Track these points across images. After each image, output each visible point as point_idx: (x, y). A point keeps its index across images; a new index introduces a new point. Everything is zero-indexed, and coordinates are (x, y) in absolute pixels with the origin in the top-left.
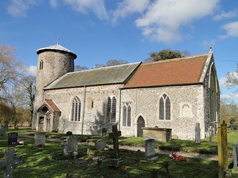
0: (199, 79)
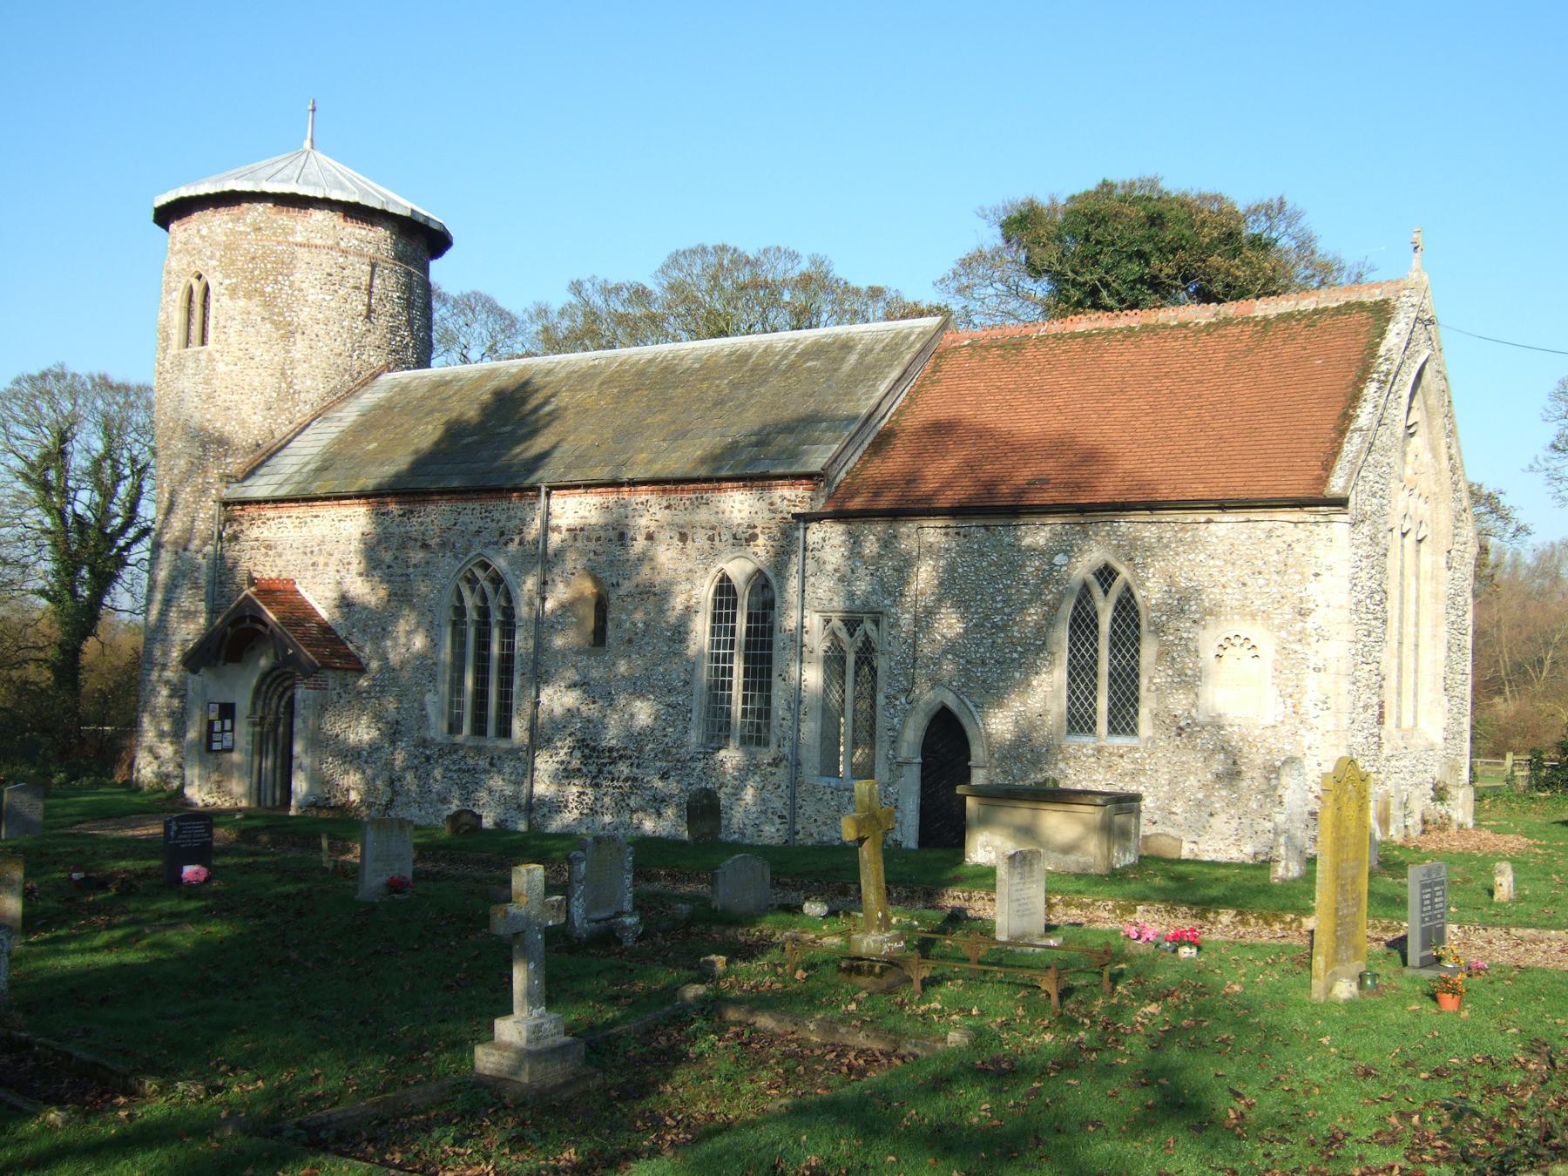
0: (1323, 481)
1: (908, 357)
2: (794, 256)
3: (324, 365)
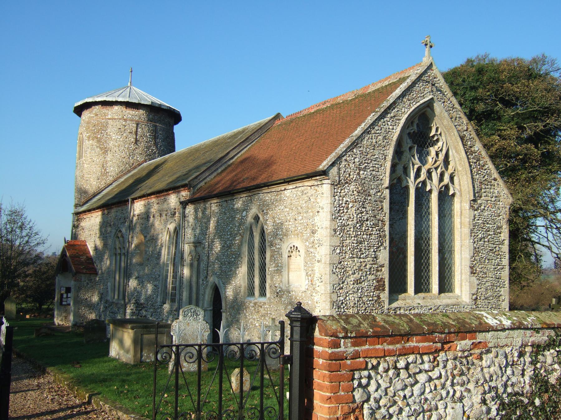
3: (118, 162)
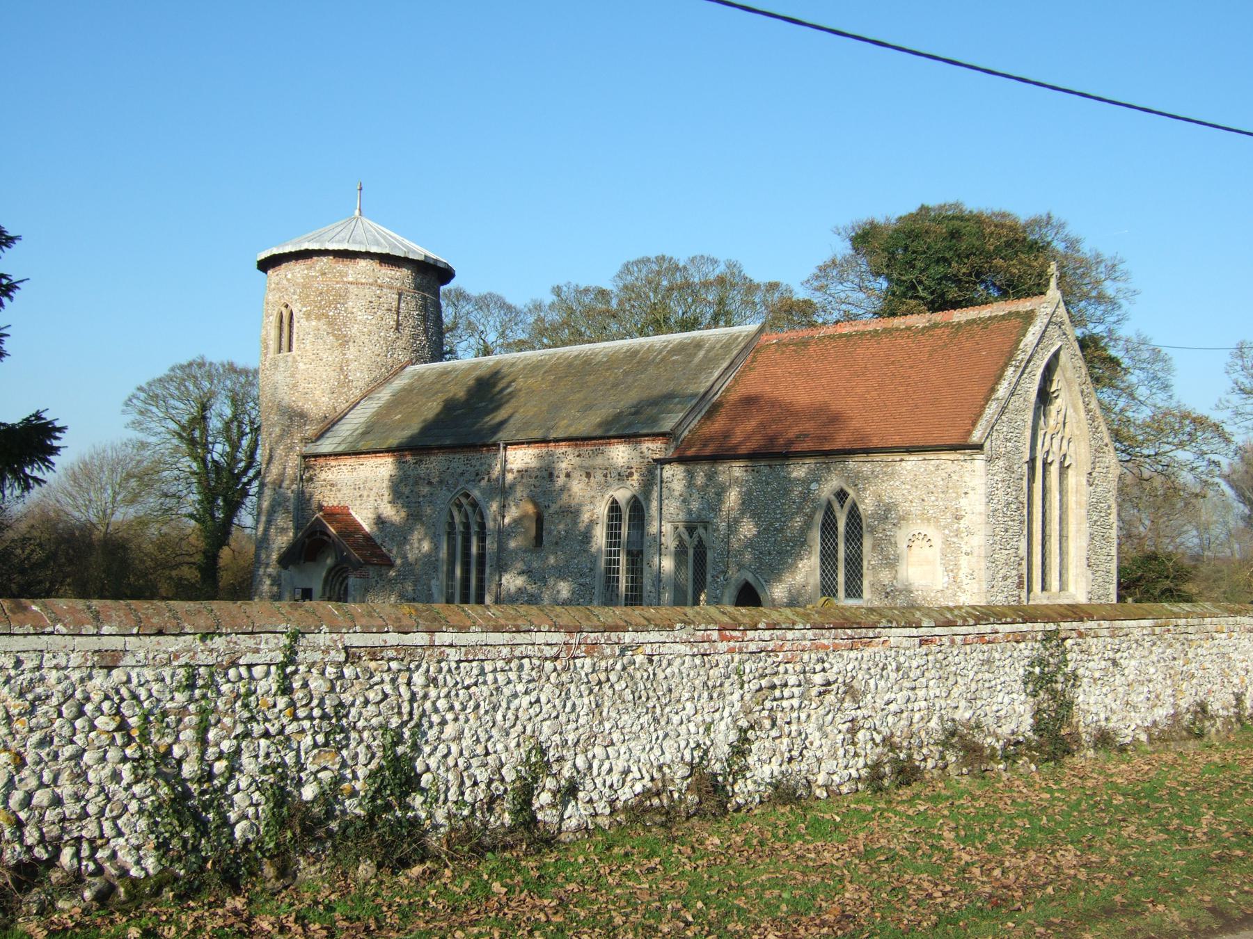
0: (969, 433)
1: (735, 353)
2: (714, 262)
